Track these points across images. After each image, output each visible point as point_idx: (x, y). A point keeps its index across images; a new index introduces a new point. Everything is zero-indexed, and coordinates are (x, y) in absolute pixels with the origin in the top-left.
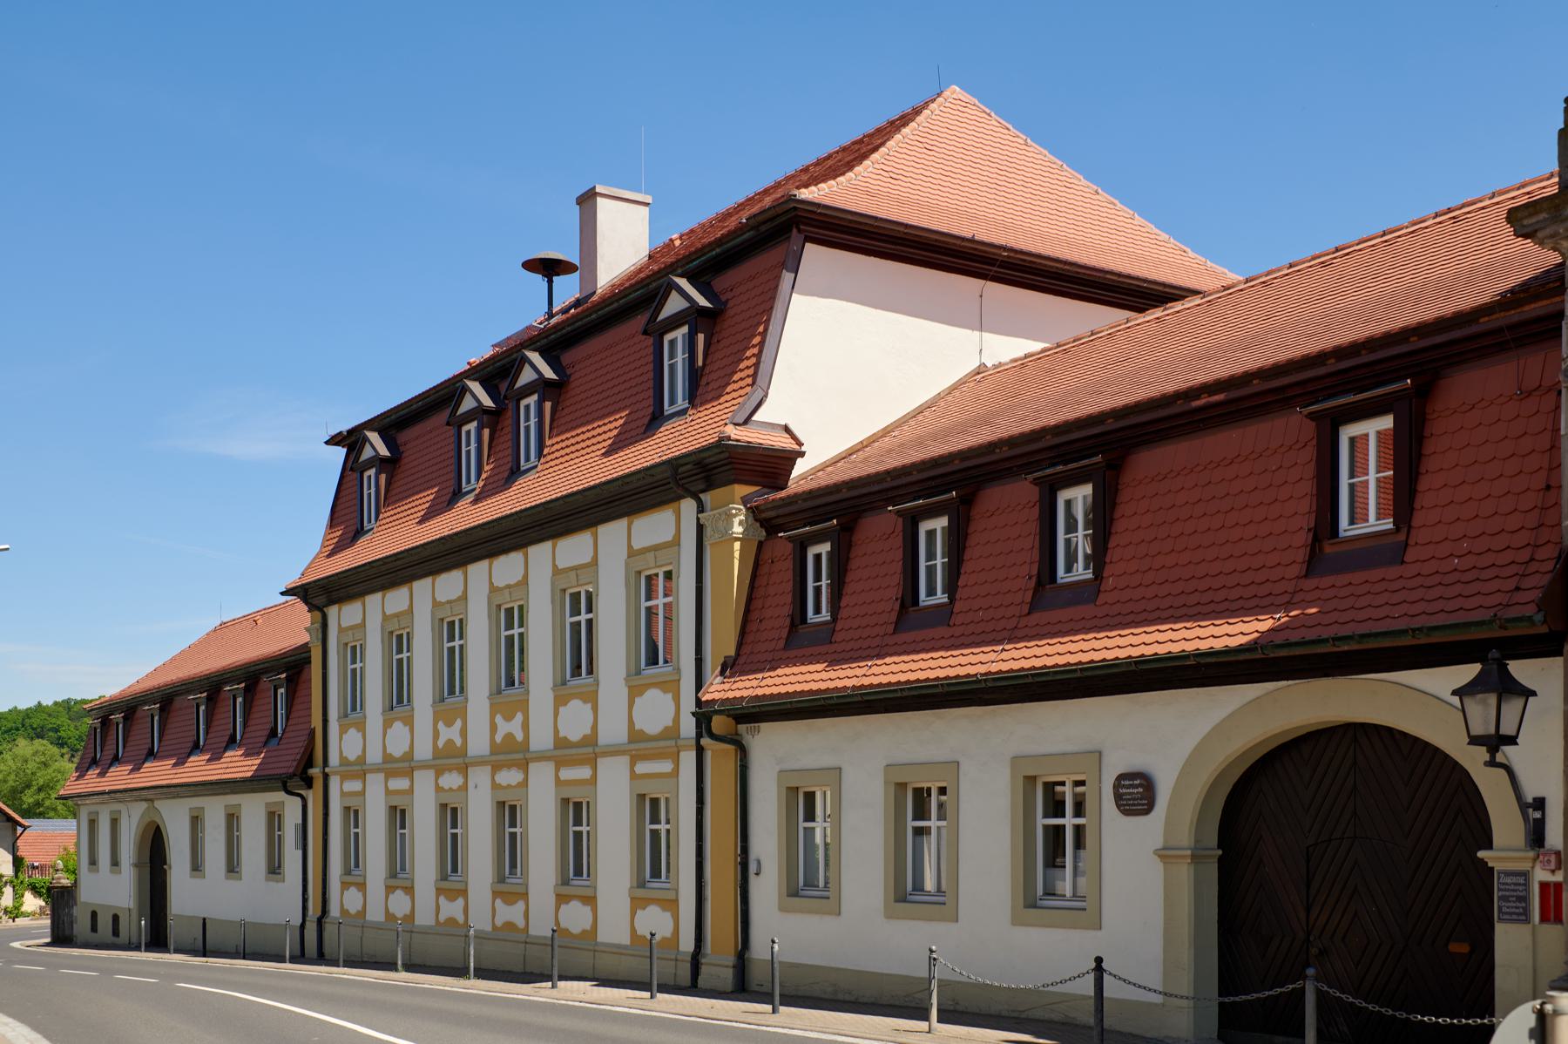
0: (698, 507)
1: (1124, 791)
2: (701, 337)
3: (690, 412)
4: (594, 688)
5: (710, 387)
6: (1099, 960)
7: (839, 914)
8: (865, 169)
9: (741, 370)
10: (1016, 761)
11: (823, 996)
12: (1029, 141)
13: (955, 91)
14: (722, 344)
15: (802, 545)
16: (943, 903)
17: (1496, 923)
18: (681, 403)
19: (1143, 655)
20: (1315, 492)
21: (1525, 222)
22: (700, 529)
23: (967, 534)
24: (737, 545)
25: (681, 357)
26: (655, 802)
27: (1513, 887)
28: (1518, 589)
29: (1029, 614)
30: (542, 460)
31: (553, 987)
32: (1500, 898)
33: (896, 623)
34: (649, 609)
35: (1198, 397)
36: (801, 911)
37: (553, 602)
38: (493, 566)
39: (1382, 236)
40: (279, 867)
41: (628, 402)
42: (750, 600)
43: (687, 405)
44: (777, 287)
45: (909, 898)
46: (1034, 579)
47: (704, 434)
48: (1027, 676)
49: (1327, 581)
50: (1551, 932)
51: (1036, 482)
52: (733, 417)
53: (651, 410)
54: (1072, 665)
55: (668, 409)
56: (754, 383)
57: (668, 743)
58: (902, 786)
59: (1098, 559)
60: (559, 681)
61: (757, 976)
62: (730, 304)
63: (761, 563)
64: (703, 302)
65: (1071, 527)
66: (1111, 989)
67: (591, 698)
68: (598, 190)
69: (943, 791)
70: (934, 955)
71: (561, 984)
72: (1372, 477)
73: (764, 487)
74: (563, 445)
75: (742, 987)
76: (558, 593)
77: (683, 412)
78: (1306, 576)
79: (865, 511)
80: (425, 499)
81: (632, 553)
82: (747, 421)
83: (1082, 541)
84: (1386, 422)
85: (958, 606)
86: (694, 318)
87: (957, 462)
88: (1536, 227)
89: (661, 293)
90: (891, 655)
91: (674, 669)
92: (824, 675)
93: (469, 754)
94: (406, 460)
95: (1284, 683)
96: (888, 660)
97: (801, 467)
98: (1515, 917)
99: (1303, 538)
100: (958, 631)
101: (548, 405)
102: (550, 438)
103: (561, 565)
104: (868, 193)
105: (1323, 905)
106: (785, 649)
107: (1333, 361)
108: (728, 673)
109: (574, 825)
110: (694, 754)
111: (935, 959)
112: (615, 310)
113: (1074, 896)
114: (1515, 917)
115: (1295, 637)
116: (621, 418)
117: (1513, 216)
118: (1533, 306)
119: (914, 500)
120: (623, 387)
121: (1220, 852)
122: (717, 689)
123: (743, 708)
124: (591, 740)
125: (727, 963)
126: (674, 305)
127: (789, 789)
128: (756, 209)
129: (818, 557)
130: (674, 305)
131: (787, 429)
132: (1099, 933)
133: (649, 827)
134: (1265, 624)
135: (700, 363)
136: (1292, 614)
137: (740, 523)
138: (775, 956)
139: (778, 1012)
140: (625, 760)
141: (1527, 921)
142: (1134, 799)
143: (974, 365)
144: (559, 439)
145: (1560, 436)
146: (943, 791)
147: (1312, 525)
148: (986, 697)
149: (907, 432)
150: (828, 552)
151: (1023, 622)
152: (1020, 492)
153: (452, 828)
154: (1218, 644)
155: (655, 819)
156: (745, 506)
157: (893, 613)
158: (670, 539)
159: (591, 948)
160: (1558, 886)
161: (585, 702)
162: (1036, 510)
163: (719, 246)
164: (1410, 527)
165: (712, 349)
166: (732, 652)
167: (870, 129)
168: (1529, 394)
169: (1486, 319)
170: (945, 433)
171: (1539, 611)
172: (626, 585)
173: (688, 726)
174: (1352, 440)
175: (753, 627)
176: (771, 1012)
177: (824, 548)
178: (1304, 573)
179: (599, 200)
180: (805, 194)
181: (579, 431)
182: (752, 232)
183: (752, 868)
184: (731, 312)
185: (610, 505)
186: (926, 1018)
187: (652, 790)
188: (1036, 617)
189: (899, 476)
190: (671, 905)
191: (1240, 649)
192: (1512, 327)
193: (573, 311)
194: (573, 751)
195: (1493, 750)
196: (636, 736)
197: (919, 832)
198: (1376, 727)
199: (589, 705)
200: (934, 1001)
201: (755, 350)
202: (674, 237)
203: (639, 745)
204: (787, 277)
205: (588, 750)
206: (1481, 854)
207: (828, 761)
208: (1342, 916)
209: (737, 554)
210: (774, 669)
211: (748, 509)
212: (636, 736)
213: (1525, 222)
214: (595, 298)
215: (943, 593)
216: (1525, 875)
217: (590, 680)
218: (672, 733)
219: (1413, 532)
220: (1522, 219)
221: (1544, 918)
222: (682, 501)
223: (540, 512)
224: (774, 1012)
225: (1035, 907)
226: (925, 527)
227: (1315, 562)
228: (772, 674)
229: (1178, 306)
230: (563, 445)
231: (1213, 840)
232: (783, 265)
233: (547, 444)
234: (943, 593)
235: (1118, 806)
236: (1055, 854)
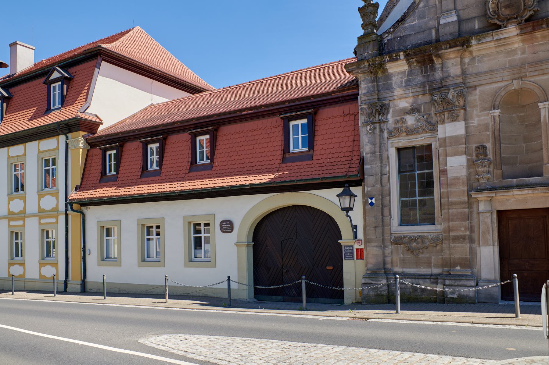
0: (66, 138)
1: (224, 226)
2: (65, 86)
3: (62, 108)
4: (25, 195)
5: (69, 101)
6: (229, 277)
7: (121, 266)
8: (117, 42)
9: (81, 97)
10: (185, 217)
11: (115, 292)
14: (73, 89)
15: (104, 151)
16: (159, 260)
17: (343, 260)
18: (58, 106)
19: (232, 185)
20: (283, 139)
21: (349, 68)
22: (67, 145)
23: (165, 149)
24: (81, 150)
25: (57, 92)
26: (17, 234)
27: (349, 250)
28: (350, 167)
29: (189, 173)
30: (3, 122)
31: (12, 294)
32: (345, 253)
33: (141, 175)
34: (15, 175)
35: (244, 111)
36: (106, 266)
37: (8, 167)
38: (40, 144)
39: (322, 66)
41: (37, 105)
42: (85, 168)
43: (60, 107)
44: (93, 73)
45: (105, 260)
46: (141, 169)
47: (23, 127)
48: (199, 190)
49: (289, 165)
50: (360, 262)
51: (190, 134)
52: (80, 110)
53: (46, 107)
54: (199, 189)
55: (52, 108)
56: (86, 101)
57: (54, 213)
58: (103, 227)
59: (160, 163)
60: (10, 193)
61: (89, 287)
62: (76, 77)
63: (88, 156)
64: (5, 94)
65: (152, 154)
66: (234, 286)
67: (24, 199)
68: (18, 42)
69: (158, 227)
70: (167, 278)
71: (15, 293)
72: (300, 136)
73: (89, 133)
74: (11, 117)
75: (84, 290)
76: (40, 159)
77: (59, 108)
78: (282, 163)
79: (319, 107)
80: (32, 111)
81: (39, 152)
82: (84, 112)
83: (156, 158)
84: (208, 137)
85: (163, 170)
86: (63, 80)
87: (120, 134)
88: (353, 70)
89: (50, 72)
90: (140, 185)
91: (56, 189)
92: (116, 191)
93: (26, 213)
94: (14, 99)
95: (276, 194)
96: (139, 186)
97: (101, 128)
98: (349, 258)
99: (280, 153)
100: (164, 178)
101: (5, 104)
102: (5, 115)
103: (41, 149)
104: (120, 50)
105: (287, 257)
106: (99, 183)
107: (287, 103)
108: (78, 190)
109: (46, 239)
110: (64, 216)
111: (167, 279)
112: (81, 58)
113: (156, 258)
114: (349, 258)
116: (34, 109)
117: (346, 66)
118: (347, 92)
119: (147, 138)
120: (34, 100)
121: (254, 243)
122: (74, 195)
123: (86, 201)
124: (23, 212)
125: (78, 283)
126: (55, 75)
127: (101, 227)
128: (87, 48)
129: (110, 155)
130: (55, 75)
131: (96, 116)
132: (215, 269)
133: (45, 240)
134: (273, 177)
135: (65, 94)
136: (280, 173)
137: (82, 143)
138: (105, 280)
140: (37, 218)
141: (353, 259)
142: (227, 228)
144: (9, 115)
145: (359, 126)
146: (158, 227)
147: (283, 149)
148: (175, 198)
149: (133, 120)
150: (114, 154)
151: (187, 175)
154: (258, 182)
155: (17, 238)
156: (84, 138)
157: (139, 172)
158: (55, 148)
159: (23, 280)
160: (361, 249)
161: (21, 200)
162: (190, 142)
163: (71, 59)
164: (313, 150)
165: (69, 90)
166: (79, 184)
167: (114, 34)
168: (346, 115)
169: (334, 94)
170: (143, 122)
171: (359, 173)
172: (37, 162)
173: (62, 207)
174: (200, 140)
175: (86, 176)
177: (113, 152)
178: (281, 162)
179: (18, 46)
180: (104, 46)
181: (18, 113)
182: (84, 56)
183: (87, 252)
184: (75, 79)
185: (32, 136)
186: (165, 298)
187: (16, 230)
188: (191, 174)
189: (140, 131)
190: (55, 265)
191: (265, 183)
192: (342, 97)
193: (7, 78)
194: (47, 213)
195: (347, 212)
196: (41, 211)
197: (148, 240)
198: (306, 206)
199: (22, 201)
200: (167, 292)
201: (86, 91)
202: (43, 60)
203: (42, 213)
204: (97, 70)
205: (23, 215)
206: (339, 241)
207: (117, 218)
208: (293, 261)
209: (81, 153)
210: (137, 185)
211: (84, 139)
212: (41, 211)
213: (349, 68)
214: (16, 75)
215: (114, 172)
216: (352, 246)
217: (22, 192)
218: (56, 210)
219: (315, 152)
220: (348, 67)
221: (357, 258)
222: (59, 136)
223: (4, 138)
224: (104, 299)
225: (104, 261)
226: (108, 153)
227: (284, 160)
228: (95, 190)
229: (204, 93)
230: (11, 117)
231: (251, 240)
232: (95, 66)
233: (5, 116)
234: (114, 172)
235: (221, 230)
236: (198, 243)
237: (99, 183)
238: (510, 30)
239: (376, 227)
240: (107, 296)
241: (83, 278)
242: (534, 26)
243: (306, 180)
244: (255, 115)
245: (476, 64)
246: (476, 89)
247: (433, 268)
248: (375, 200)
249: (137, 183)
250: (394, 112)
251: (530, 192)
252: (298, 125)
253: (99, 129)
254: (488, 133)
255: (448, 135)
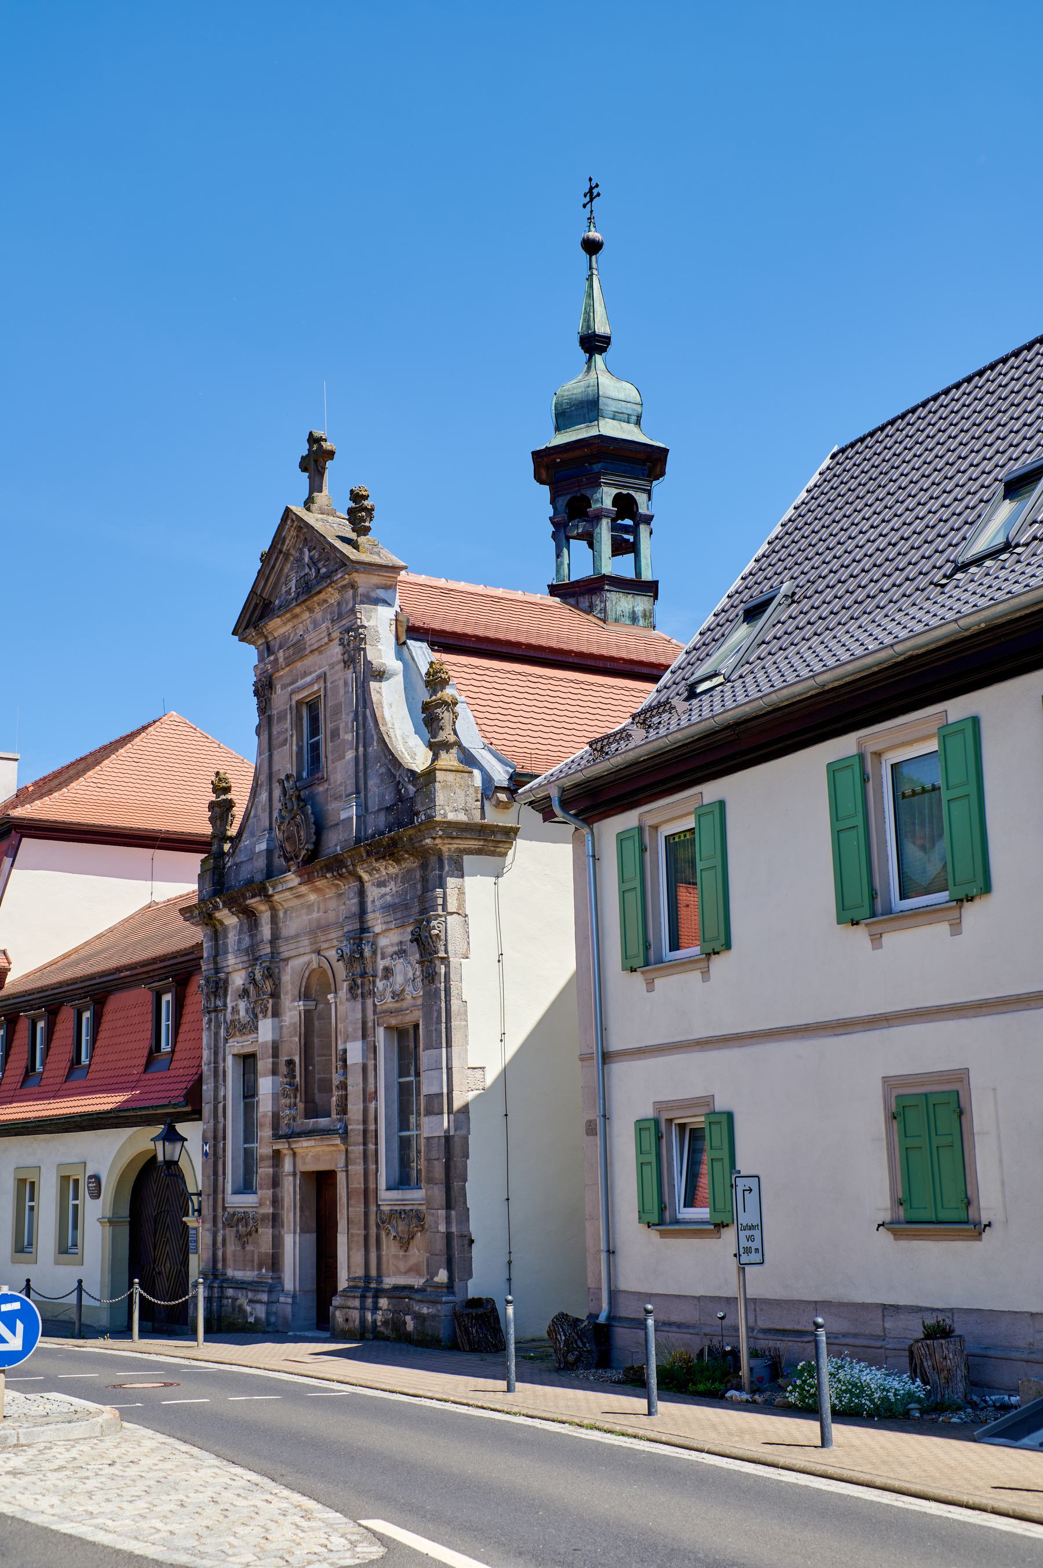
4: (958, 921)
6: (80, 1282)
12: (221, 745)
13: (172, 715)
40: (30, 1244)
45: (70, 1251)
66: (86, 1301)
71: (840, 1432)
115: (134, 1105)
139: (514, 1391)
143: (147, 902)
152: (142, 995)
153: (74, 1199)
176: (505, 1389)
180: (18, 812)
188: (24, 1091)
191: (111, 1111)
206: (184, 1219)
225: (67, 1253)
237: (144, 1072)
238: (287, 878)
240: (660, 1399)
243: (141, 1108)
244: (134, 978)
249: (15, 1099)
251: (312, 1143)
253: (8, 980)
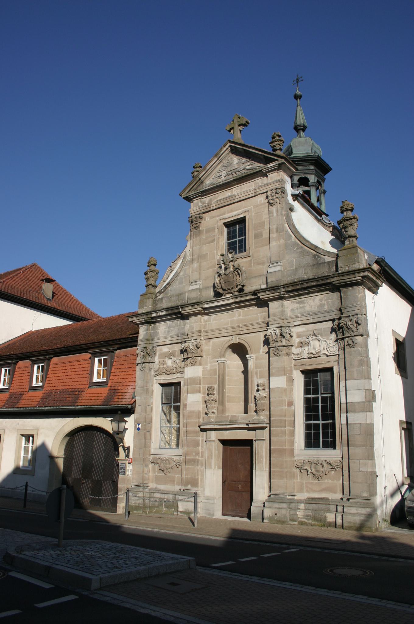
6: (27, 483)
206: (117, 458)
239: (140, 448)
241: (328, 292)
242: (77, 398)
245: (211, 322)
246: (210, 341)
247: (176, 485)
248: (141, 426)
250: (159, 355)
252: (101, 359)
254: (216, 376)
255: (189, 376)
